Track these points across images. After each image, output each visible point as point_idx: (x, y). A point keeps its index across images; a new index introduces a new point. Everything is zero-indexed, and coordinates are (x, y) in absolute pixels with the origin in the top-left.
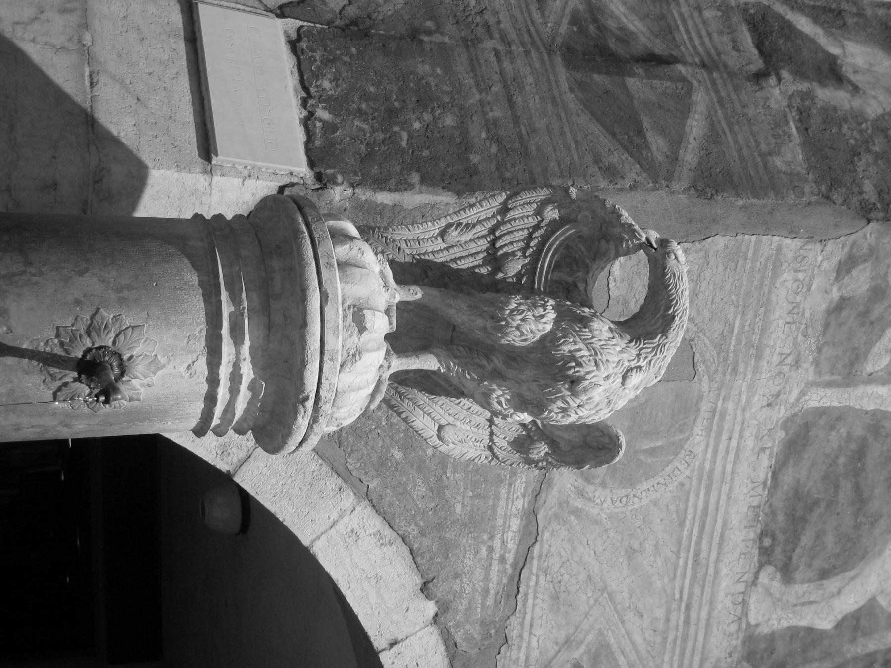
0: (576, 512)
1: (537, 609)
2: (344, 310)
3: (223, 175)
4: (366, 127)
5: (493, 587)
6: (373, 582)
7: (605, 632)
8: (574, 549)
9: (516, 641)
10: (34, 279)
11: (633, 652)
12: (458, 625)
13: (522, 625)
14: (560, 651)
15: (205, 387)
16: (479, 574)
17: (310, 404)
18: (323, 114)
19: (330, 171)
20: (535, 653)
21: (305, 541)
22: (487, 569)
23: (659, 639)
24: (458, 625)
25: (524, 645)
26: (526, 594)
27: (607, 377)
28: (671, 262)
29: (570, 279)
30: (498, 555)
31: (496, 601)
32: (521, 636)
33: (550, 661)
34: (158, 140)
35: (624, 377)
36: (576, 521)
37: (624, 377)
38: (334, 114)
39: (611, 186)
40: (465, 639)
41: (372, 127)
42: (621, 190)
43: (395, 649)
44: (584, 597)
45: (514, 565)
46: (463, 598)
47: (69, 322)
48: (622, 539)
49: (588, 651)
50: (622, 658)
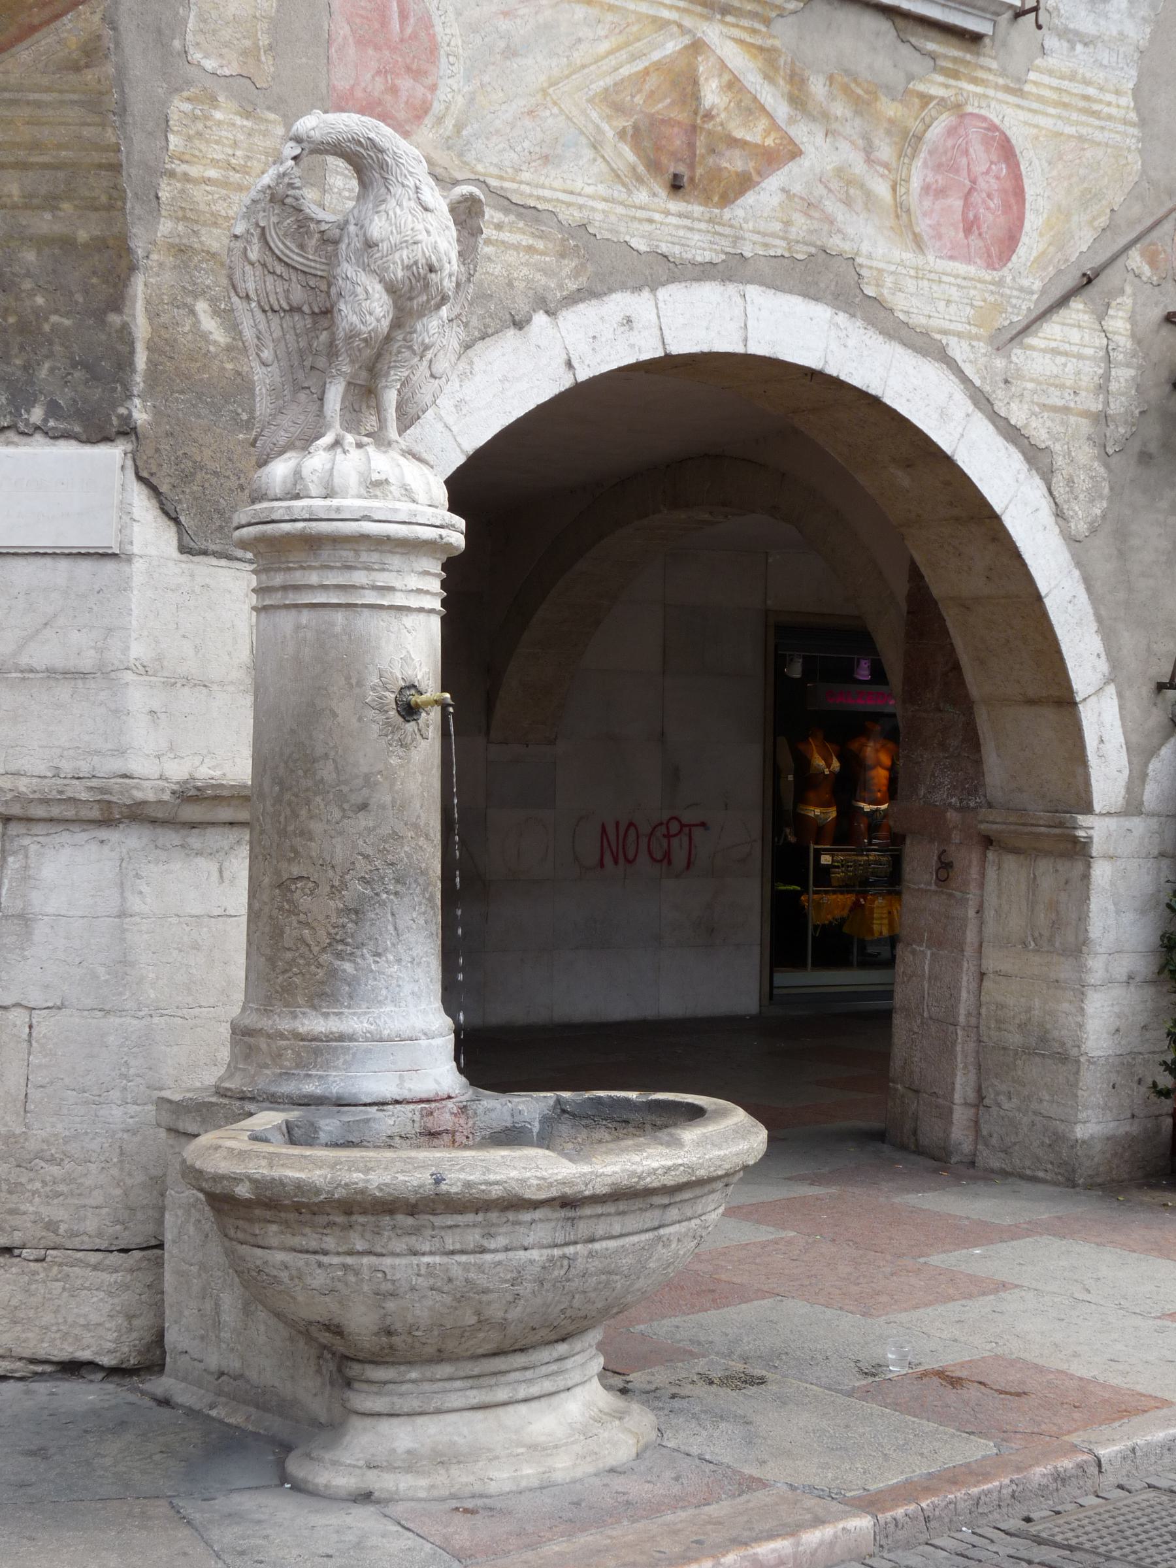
0: (459, 127)
1: (556, 184)
2: (371, 497)
3: (131, 543)
4: (47, 365)
5: (527, 241)
6: (507, 385)
7: (591, 93)
8: (497, 131)
9: (586, 213)
10: (340, 752)
11: (618, 54)
12: (561, 286)
13: (569, 205)
14: (603, 157)
15: (422, 616)
16: (511, 257)
17: (443, 532)
18: (37, 415)
19: (115, 421)
20: (602, 189)
21: (460, 460)
22: (506, 245)
23: (609, 17)
24: (561, 286)
25: (590, 203)
26: (539, 198)
27: (428, 232)
28: (316, 135)
29: (317, 236)
30: (494, 232)
31: (541, 237)
32: (581, 207)
33: (613, 170)
34: (95, 608)
35: (426, 209)
36: (469, 128)
37: (426, 209)
38: (35, 401)
39: (113, 58)
40: (576, 278)
41: (47, 357)
42: (117, 44)
43: (575, 363)
44: (550, 121)
45: (506, 211)
46: (532, 280)
47: (375, 727)
48: (493, 64)
49: (609, 118)
50: (621, 70)
